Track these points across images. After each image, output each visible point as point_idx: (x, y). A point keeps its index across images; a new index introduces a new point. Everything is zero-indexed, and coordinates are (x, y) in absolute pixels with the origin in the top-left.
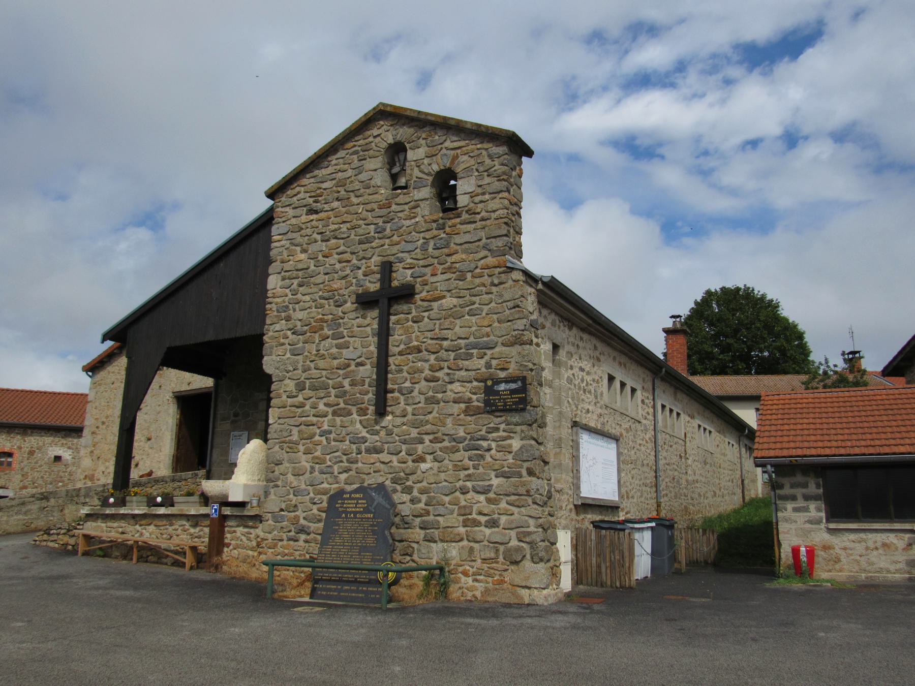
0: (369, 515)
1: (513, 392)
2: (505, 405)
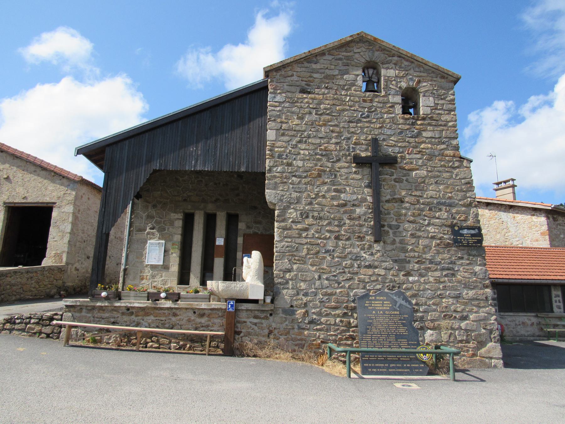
0: (396, 312)
1: (473, 235)
2: (468, 243)
